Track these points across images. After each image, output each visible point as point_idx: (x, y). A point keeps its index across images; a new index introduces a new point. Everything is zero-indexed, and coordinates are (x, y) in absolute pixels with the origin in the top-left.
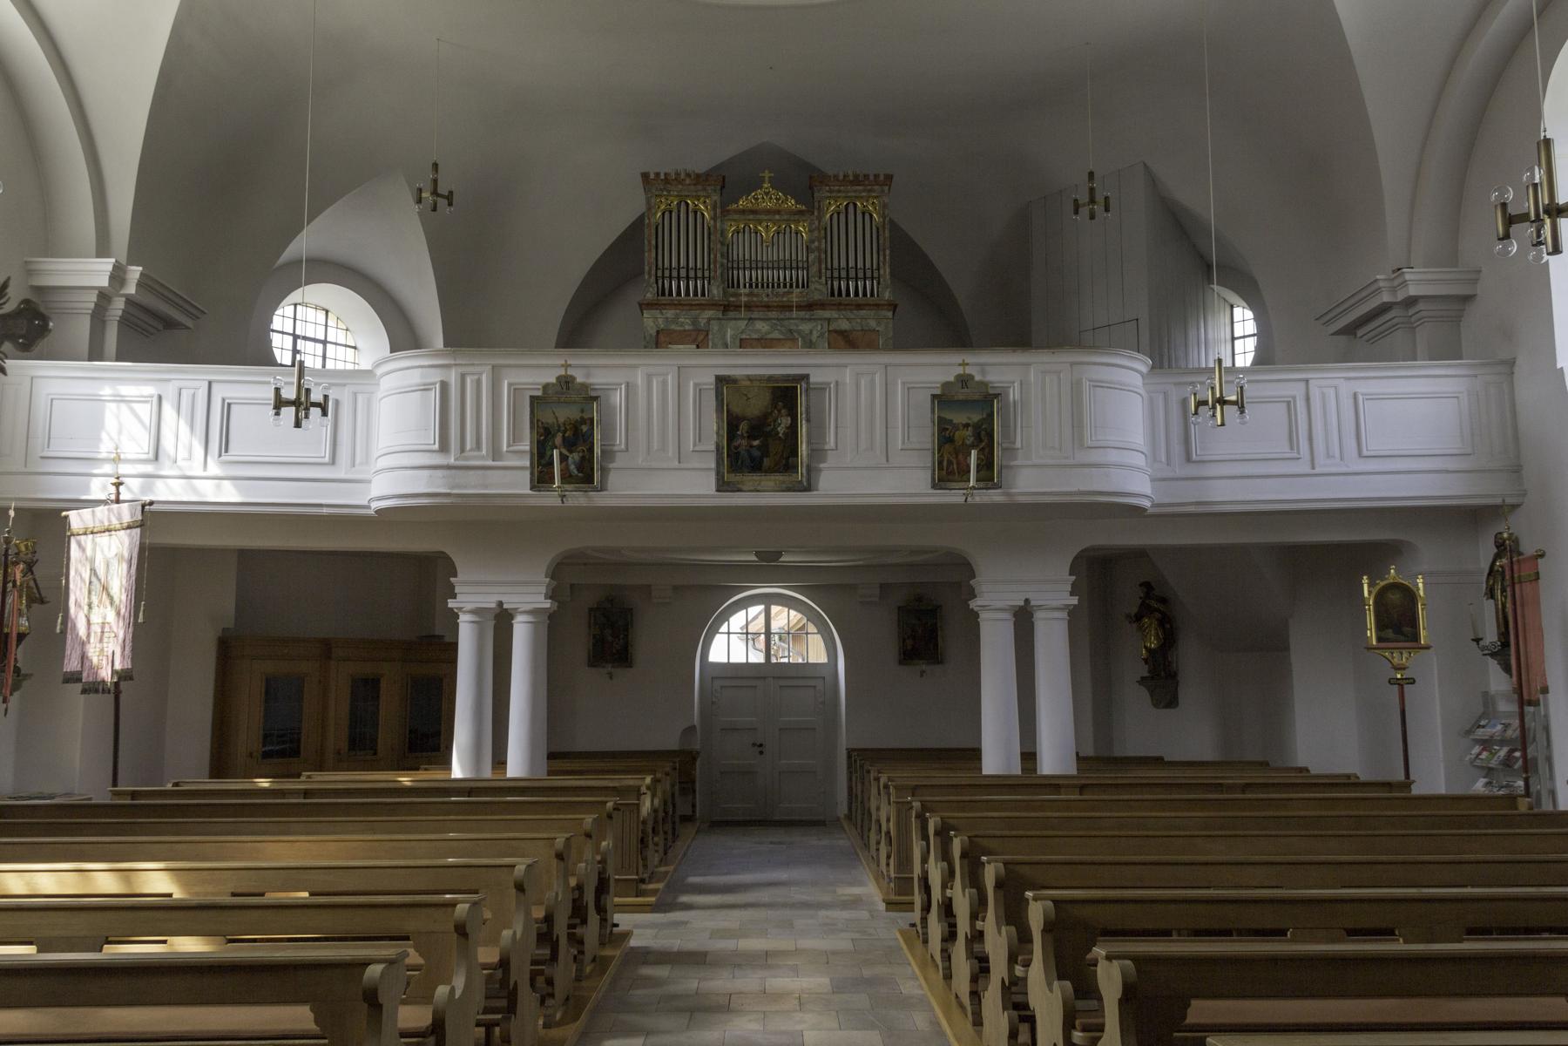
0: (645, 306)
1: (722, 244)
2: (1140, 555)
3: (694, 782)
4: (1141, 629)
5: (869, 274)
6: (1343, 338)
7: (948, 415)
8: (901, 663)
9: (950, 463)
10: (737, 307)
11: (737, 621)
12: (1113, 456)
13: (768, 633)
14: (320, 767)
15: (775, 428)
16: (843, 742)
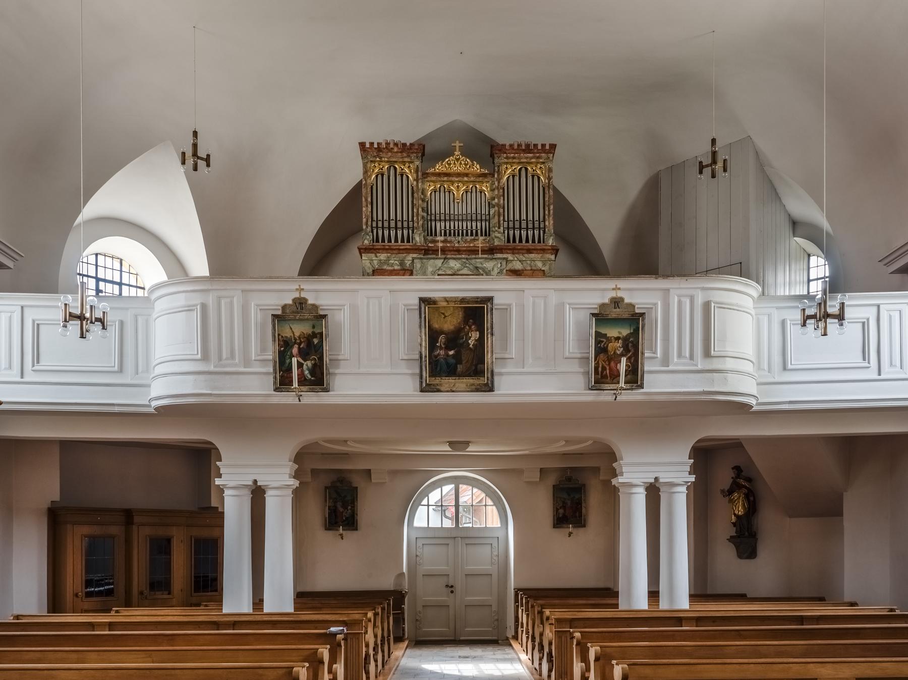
0: (363, 250)
1: (423, 200)
2: (736, 445)
3: (403, 613)
4: (731, 501)
5: (536, 225)
6: (898, 276)
7: (603, 331)
8: (554, 527)
9: (604, 368)
10: (435, 251)
11: (435, 496)
12: (729, 364)
13: (457, 506)
14: (128, 604)
15: (467, 340)
16: (512, 584)
